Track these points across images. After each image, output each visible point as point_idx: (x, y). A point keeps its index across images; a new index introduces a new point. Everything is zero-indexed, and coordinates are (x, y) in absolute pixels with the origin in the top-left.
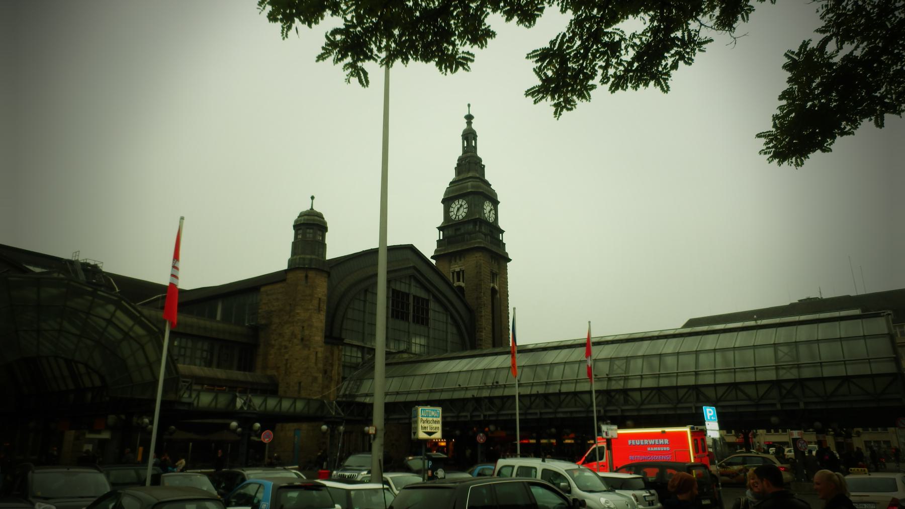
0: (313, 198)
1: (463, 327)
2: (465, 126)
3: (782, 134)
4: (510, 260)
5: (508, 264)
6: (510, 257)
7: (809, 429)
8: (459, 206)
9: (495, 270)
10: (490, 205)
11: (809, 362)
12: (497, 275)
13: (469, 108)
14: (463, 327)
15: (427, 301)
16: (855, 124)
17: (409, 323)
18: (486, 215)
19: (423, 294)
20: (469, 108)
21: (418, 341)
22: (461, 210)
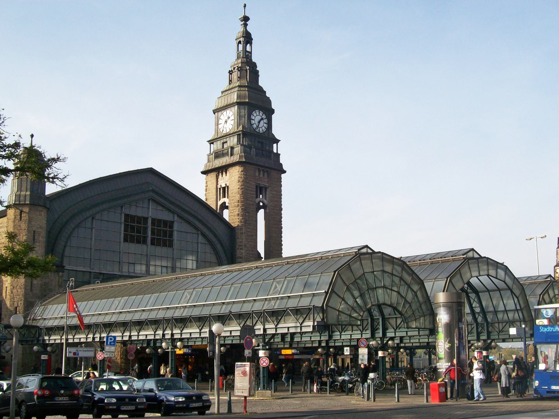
0: (32, 136)
1: (219, 247)
2: (241, 29)
3: (11, 239)
4: (285, 172)
5: (283, 176)
6: (285, 168)
7: (184, 354)
8: (226, 118)
9: (264, 183)
10: (261, 114)
11: (547, 285)
12: (266, 189)
13: (245, 9)
14: (219, 247)
15: (172, 222)
16: (242, 167)
17: (147, 246)
18: (255, 126)
19: (165, 216)
20: (245, 9)
21: (158, 263)
22: (229, 121)
